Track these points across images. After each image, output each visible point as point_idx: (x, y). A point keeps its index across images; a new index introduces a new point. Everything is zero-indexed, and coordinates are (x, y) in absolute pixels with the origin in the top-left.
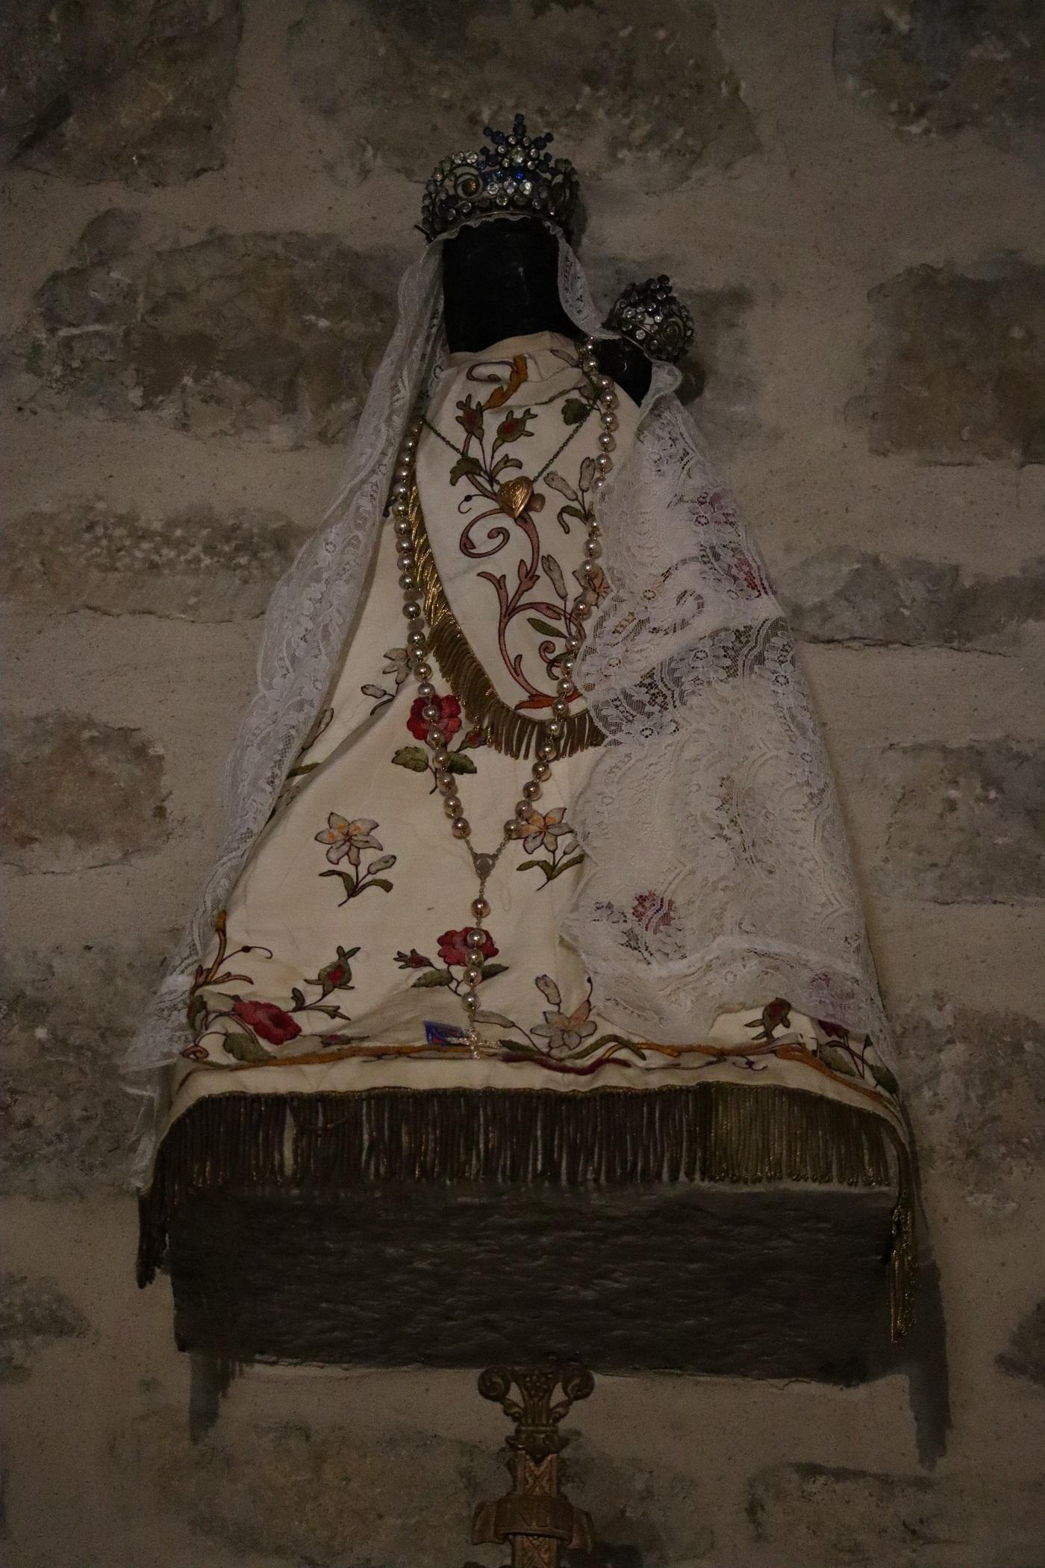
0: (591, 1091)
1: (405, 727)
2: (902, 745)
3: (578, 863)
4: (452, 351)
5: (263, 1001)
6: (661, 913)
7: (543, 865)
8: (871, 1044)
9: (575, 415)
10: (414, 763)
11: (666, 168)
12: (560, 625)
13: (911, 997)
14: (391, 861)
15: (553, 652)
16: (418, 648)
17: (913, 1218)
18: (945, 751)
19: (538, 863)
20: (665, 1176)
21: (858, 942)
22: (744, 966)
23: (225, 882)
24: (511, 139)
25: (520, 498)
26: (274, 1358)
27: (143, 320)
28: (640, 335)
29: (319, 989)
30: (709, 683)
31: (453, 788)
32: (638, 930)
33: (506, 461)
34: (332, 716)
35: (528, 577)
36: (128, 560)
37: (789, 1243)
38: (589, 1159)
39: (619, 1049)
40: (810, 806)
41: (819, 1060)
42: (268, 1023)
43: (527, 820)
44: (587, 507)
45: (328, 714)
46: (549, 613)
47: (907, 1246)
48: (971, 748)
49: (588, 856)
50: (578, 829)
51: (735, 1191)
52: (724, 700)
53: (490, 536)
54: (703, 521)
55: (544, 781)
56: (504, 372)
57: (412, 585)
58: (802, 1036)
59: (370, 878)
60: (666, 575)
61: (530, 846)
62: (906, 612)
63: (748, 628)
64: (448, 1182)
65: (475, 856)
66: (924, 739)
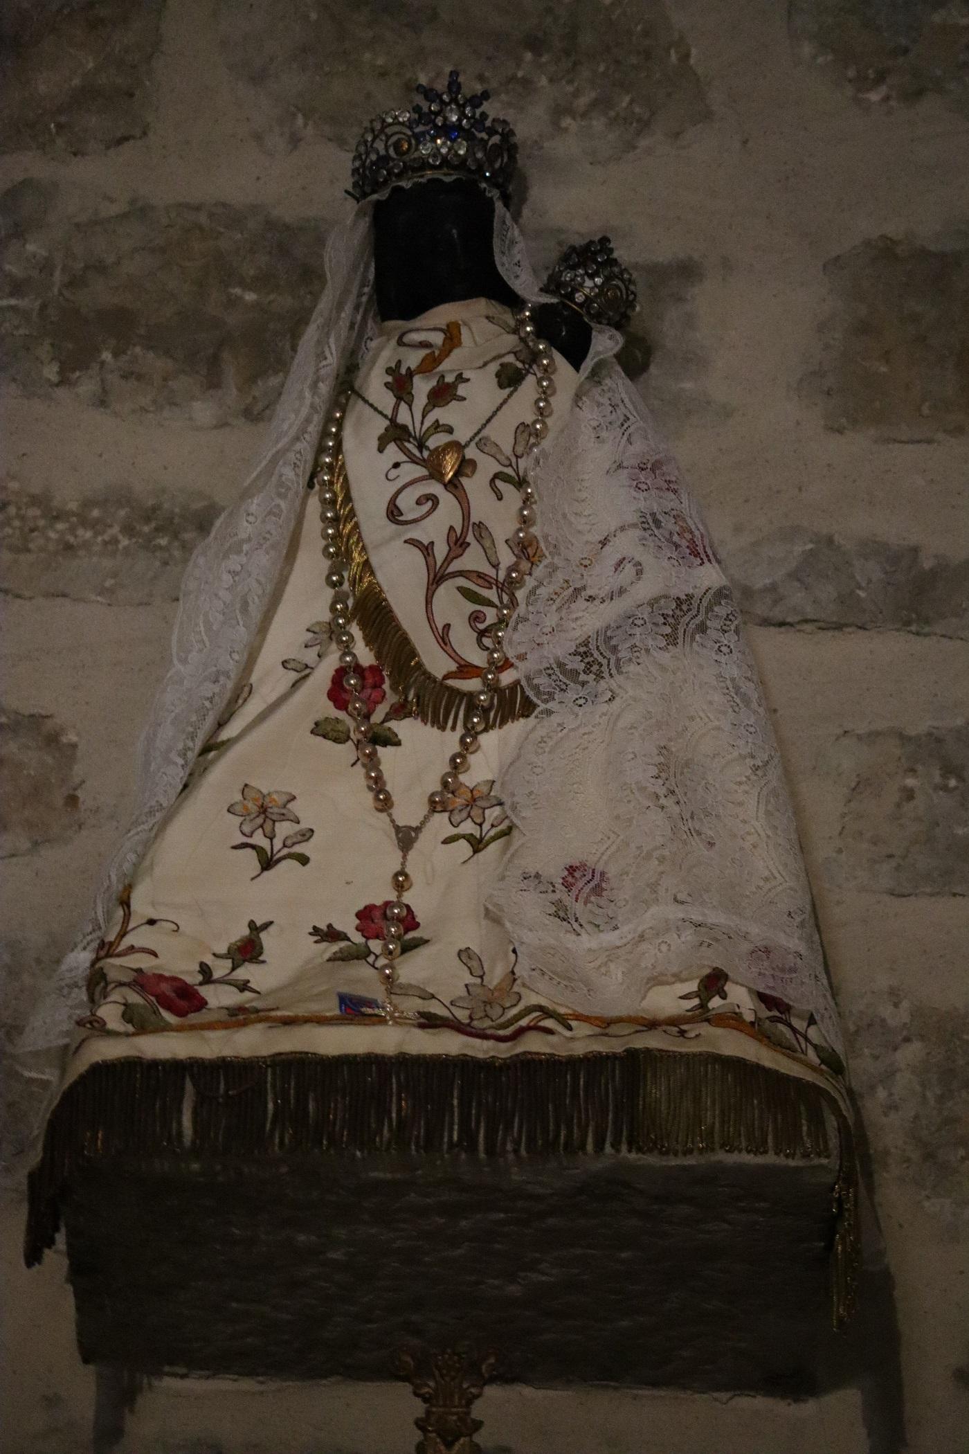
0: (511, 1058)
1: (325, 697)
2: (857, 732)
4: (383, 320)
5: (167, 974)
6: (592, 884)
7: (469, 838)
9: (510, 379)
10: (335, 734)
11: (611, 136)
12: (491, 594)
14: (308, 835)
16: (340, 617)
17: (856, 1196)
18: (903, 738)
19: (464, 837)
20: (590, 1147)
21: (803, 917)
23: (132, 857)
24: (445, 97)
26: (183, 1371)
27: (61, 294)
28: (579, 297)
30: (647, 651)
31: (375, 759)
32: (568, 900)
33: (437, 427)
34: (250, 692)
35: (458, 544)
36: (41, 542)
37: (726, 1226)
38: (509, 1127)
39: (543, 1019)
40: (753, 778)
41: (755, 1030)
43: (453, 793)
45: (247, 689)
46: (480, 581)
47: (849, 1224)
48: (930, 734)
49: (517, 827)
50: (504, 798)
51: (664, 1163)
52: (663, 668)
53: (419, 502)
54: (644, 487)
55: (472, 753)
56: (437, 339)
57: (337, 554)
58: (739, 1007)
59: (285, 851)
60: (604, 543)
61: (456, 818)
62: (862, 594)
63: (690, 597)
64: (358, 1153)
65: (398, 829)
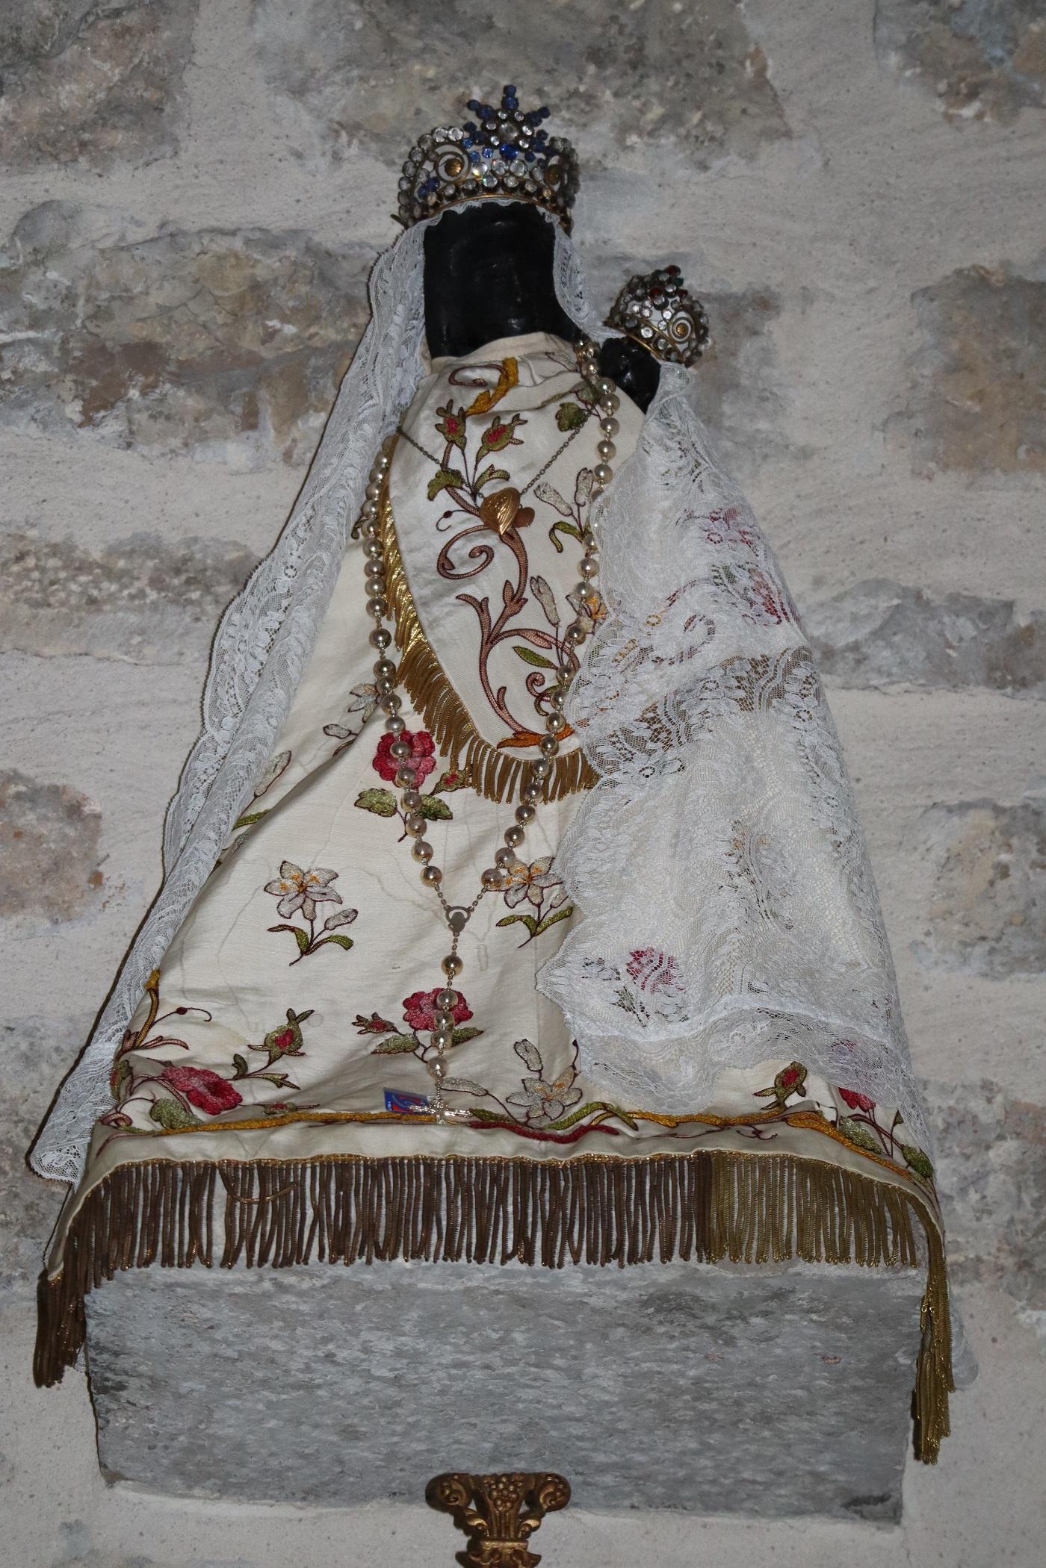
3: (566, 916)
6: (660, 970)
7: (527, 920)
8: (901, 1122)
9: (571, 421)
12: (551, 655)
13: (956, 1087)
14: (352, 916)
15: (543, 684)
18: (998, 811)
19: (520, 918)
22: (754, 1028)
25: (504, 514)
27: (84, 326)
29: (265, 1057)
35: (514, 600)
36: (63, 595)
42: (202, 1089)
44: (583, 525)
46: (539, 641)
48: (1025, 807)
59: (326, 935)
60: (672, 599)
61: (513, 898)
63: (765, 659)
66: (971, 796)
